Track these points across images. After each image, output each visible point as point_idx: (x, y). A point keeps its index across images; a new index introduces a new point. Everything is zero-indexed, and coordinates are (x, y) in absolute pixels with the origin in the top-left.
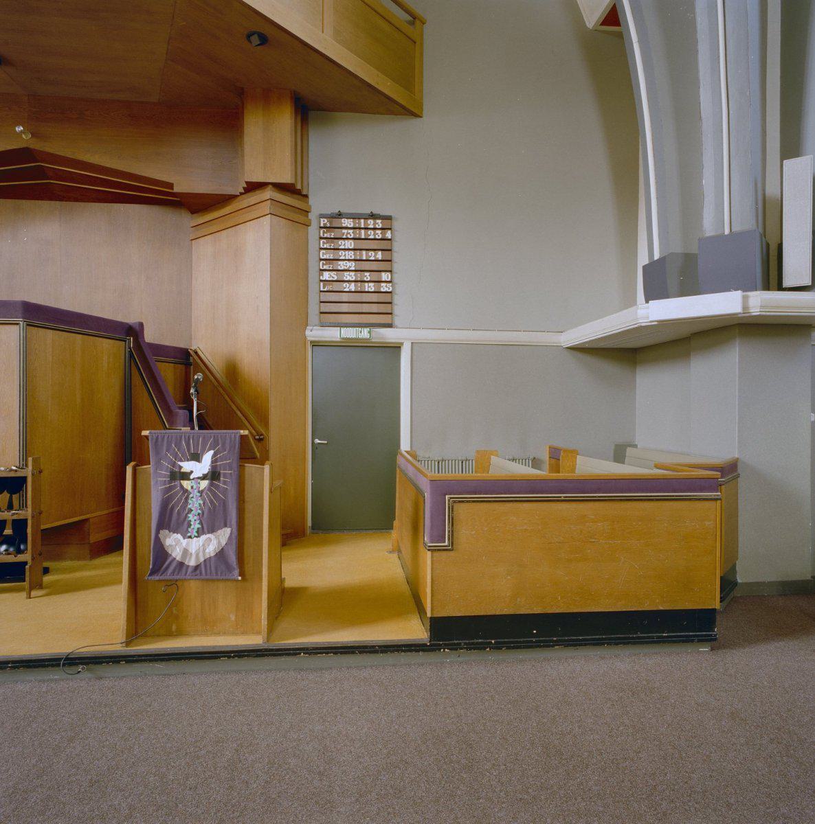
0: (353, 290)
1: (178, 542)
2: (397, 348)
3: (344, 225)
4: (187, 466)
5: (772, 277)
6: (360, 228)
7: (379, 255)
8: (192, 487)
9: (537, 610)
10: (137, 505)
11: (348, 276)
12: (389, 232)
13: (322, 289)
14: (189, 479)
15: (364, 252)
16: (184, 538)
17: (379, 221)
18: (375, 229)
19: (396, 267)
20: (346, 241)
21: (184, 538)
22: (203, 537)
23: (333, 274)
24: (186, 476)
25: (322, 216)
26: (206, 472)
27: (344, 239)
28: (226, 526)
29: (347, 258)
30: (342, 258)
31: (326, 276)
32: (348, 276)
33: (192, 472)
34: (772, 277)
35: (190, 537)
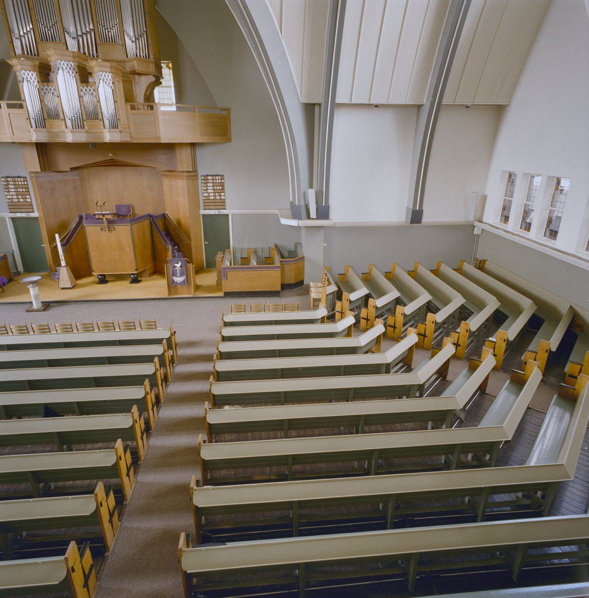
2: (227, 216)
4: (176, 265)
5: (309, 217)
7: (220, 188)
10: (219, 299)
24: (176, 267)
31: (205, 195)
34: (309, 217)
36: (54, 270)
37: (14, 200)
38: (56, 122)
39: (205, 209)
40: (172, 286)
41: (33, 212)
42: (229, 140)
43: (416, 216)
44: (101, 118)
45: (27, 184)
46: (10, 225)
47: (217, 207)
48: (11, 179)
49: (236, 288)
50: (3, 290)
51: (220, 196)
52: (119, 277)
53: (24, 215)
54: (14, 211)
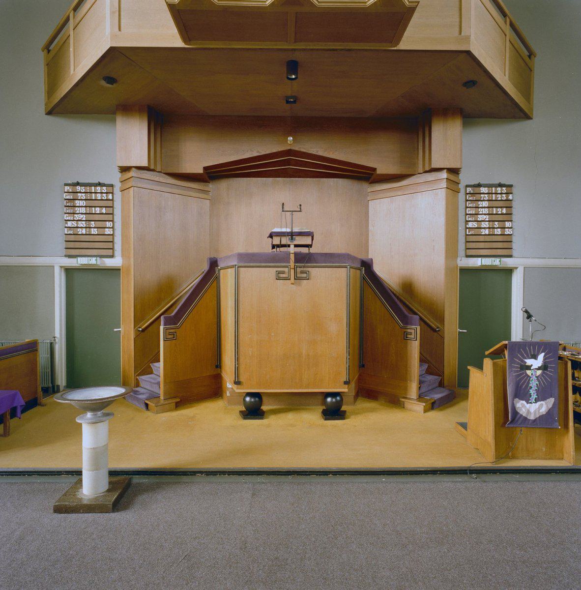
0: (487, 234)
1: (523, 406)
2: (509, 272)
3: (482, 192)
4: (529, 362)
6: (492, 193)
7: (504, 211)
8: (532, 374)
11: (484, 225)
12: (511, 195)
13: (468, 233)
14: (530, 369)
15: (494, 209)
16: (527, 404)
17: (504, 188)
18: (501, 193)
20: (483, 202)
21: (527, 404)
22: (539, 403)
23: (474, 223)
24: (529, 368)
25: (467, 186)
26: (540, 365)
27: (481, 201)
28: (551, 397)
29: (484, 213)
30: (481, 213)
31: (470, 225)
32: (484, 225)
33: (532, 365)
35: (531, 403)
36: (133, 383)
37: (80, 231)
39: (467, 256)
41: (112, 256)
45: (112, 200)
46: (59, 282)
48: (83, 189)
50: (5, 427)
52: (295, 401)
54: (73, 252)
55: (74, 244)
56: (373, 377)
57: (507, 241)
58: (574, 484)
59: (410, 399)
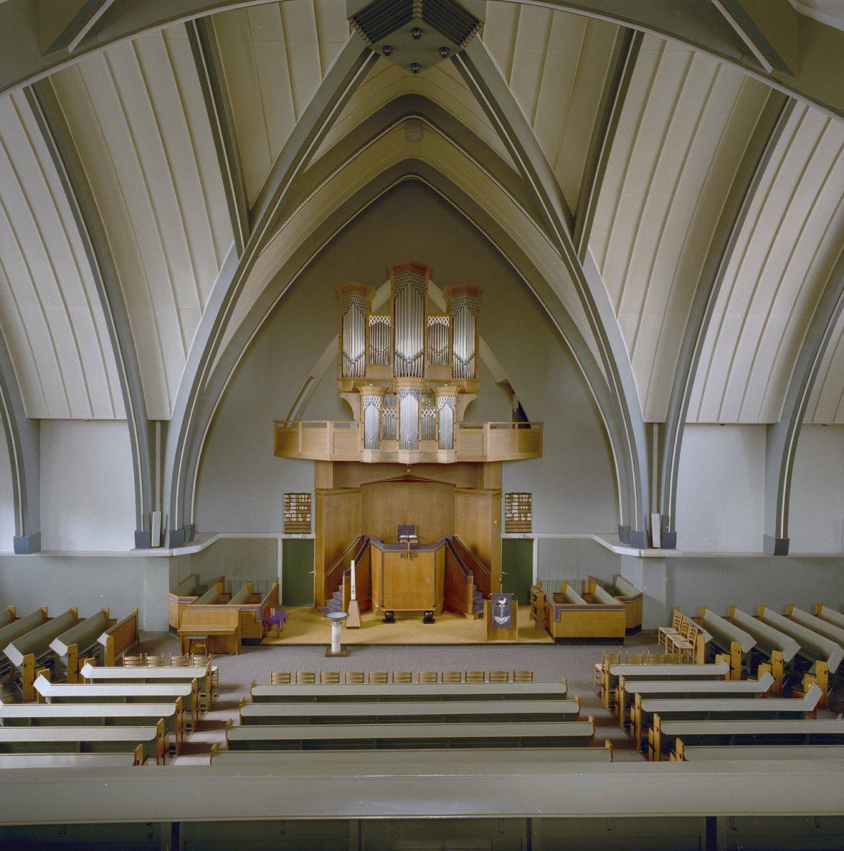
2: (531, 541)
4: (500, 602)
5: (650, 545)
9: (610, 636)
19: (533, 511)
31: (508, 515)
34: (650, 545)
36: (323, 603)
37: (293, 520)
38: (391, 443)
40: (493, 627)
41: (309, 533)
42: (540, 455)
43: (781, 547)
44: (437, 439)
47: (521, 530)
48: (294, 496)
49: (571, 633)
51: (526, 517)
53: (300, 536)
55: (289, 527)
56: (451, 603)
57: (529, 524)
58: (839, 749)
59: (468, 613)
